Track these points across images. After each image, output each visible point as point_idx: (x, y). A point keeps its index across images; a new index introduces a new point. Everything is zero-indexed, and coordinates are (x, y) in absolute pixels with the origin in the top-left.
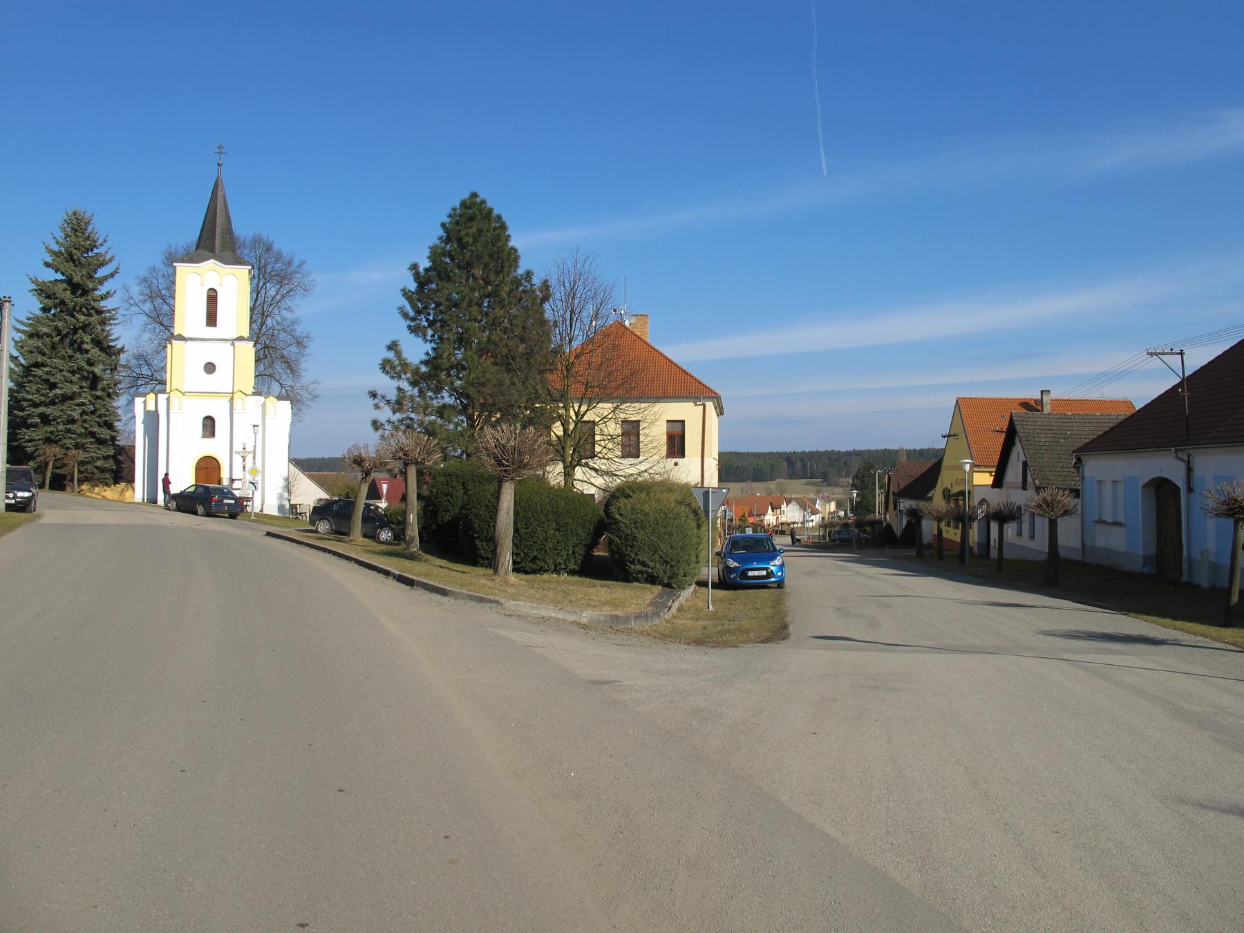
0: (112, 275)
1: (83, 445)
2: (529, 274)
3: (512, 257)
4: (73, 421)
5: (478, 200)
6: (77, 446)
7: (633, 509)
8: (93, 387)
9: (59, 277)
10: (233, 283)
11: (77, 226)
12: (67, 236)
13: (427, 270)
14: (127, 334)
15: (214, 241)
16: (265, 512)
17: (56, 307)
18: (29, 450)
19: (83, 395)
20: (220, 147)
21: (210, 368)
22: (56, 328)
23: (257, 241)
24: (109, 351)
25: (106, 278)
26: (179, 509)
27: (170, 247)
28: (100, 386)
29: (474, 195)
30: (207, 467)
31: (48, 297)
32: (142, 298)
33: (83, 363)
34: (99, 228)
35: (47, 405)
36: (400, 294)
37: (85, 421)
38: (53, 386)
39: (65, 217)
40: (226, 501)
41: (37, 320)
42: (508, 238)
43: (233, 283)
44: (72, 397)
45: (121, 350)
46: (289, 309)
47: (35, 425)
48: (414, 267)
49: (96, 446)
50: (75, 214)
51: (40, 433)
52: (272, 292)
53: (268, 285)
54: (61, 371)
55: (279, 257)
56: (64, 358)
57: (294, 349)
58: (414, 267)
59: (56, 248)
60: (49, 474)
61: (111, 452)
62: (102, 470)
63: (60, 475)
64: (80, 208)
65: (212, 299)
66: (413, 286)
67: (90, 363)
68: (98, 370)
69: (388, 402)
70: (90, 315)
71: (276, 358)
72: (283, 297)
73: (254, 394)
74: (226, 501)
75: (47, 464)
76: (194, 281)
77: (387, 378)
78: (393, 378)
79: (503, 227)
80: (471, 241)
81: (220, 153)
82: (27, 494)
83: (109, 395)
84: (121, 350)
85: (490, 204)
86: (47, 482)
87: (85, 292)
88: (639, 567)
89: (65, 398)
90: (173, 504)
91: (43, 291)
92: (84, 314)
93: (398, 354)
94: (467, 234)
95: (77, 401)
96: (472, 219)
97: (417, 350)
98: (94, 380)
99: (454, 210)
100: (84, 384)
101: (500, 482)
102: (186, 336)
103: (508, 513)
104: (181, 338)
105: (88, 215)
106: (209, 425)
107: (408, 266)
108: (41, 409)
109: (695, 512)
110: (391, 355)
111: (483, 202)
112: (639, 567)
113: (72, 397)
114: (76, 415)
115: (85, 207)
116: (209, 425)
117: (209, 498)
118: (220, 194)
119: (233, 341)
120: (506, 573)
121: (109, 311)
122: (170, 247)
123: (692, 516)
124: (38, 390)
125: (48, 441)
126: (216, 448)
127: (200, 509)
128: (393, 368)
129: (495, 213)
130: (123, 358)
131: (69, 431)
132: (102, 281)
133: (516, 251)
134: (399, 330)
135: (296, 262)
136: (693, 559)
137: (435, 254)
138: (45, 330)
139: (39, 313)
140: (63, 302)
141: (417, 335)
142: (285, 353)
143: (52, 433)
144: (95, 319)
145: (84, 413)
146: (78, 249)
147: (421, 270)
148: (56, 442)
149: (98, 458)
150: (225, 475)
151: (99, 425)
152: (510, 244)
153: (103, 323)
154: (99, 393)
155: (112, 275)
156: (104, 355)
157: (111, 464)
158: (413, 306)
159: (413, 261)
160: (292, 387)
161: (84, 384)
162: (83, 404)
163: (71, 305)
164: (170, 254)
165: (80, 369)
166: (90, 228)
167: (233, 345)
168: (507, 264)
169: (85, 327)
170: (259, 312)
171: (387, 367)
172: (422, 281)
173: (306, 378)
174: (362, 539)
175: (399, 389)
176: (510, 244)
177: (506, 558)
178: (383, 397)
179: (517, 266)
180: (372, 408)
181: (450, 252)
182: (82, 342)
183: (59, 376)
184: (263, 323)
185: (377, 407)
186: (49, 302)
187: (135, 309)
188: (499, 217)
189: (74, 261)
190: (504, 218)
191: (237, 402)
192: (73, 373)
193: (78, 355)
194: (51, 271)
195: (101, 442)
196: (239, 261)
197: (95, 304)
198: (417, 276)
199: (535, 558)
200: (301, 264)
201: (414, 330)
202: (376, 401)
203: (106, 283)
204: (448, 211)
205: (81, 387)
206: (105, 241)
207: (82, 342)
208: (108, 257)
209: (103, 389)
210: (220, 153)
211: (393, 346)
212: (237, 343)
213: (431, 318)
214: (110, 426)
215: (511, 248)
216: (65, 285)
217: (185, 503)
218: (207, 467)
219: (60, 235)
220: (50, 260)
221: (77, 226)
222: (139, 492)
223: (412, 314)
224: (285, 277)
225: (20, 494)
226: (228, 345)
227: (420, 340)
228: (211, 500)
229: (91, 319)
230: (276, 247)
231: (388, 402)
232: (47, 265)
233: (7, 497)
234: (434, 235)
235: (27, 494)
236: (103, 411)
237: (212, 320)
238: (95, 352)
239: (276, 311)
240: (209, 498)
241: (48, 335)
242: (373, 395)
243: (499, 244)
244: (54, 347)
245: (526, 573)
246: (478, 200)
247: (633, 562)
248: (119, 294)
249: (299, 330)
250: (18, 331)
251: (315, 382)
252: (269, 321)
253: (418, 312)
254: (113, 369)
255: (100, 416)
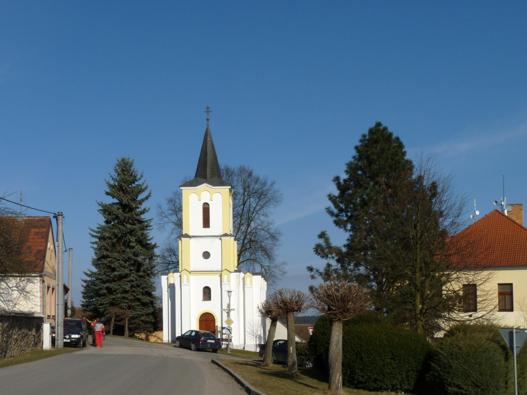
0: (147, 198)
1: (133, 307)
2: (420, 178)
3: (409, 166)
4: (126, 292)
5: (381, 128)
6: (130, 307)
7: (451, 344)
8: (138, 270)
9: (116, 201)
10: (219, 199)
11: (125, 169)
12: (119, 175)
13: (345, 180)
14: (157, 236)
15: (208, 171)
16: (246, 349)
17: (114, 221)
18: (101, 310)
19: (132, 275)
20: (208, 108)
21: (206, 255)
22: (114, 233)
23: (242, 170)
24: (149, 247)
25: (143, 200)
26: (181, 346)
27: (186, 178)
28: (142, 269)
29: (379, 124)
30: (207, 319)
31: (109, 214)
32: (170, 212)
33: (130, 255)
34: (138, 168)
35: (110, 282)
36: (327, 199)
37: (133, 292)
38: (114, 270)
39: (117, 163)
40: (209, 341)
41: (103, 229)
42: (404, 154)
43: (219, 199)
44: (126, 276)
45: (155, 246)
46: (266, 215)
47: (104, 295)
48: (337, 179)
49: (141, 307)
50: (123, 160)
51: (106, 300)
52: (254, 205)
53: (251, 199)
54: (118, 260)
55: (257, 180)
56: (119, 252)
57: (270, 241)
58: (337, 179)
59: (112, 182)
60: (112, 325)
61: (151, 310)
62: (146, 322)
63: (120, 326)
64: (126, 156)
65: (206, 209)
66: (336, 192)
67: (136, 255)
68: (140, 259)
69: (321, 274)
70: (135, 224)
71: (253, 249)
72: (262, 207)
73: (236, 271)
74: (209, 341)
75: (111, 318)
76: (194, 199)
77: (319, 257)
78: (322, 257)
79: (401, 146)
80: (375, 157)
81: (208, 112)
82: (77, 336)
83: (148, 275)
84: (155, 246)
85: (390, 130)
86: (111, 330)
87: (131, 210)
88: (455, 389)
89: (121, 277)
90: (178, 343)
91: (106, 210)
92: (130, 224)
93: (327, 240)
94: (373, 153)
95: (128, 279)
96: (376, 142)
97: (340, 238)
98: (138, 266)
99: (364, 136)
100: (132, 268)
101: (331, 322)
102: (190, 234)
103: (337, 345)
104: (187, 236)
105: (130, 160)
106: (207, 293)
107: (332, 178)
108: (107, 285)
109: (504, 348)
110: (321, 241)
111: (385, 129)
112: (455, 389)
113: (126, 276)
114: (128, 288)
115: (129, 155)
116: (207, 293)
117: (205, 339)
118: (209, 139)
119: (220, 237)
120: (337, 388)
121: (146, 221)
122: (186, 178)
123: (500, 350)
124: (105, 273)
125: (112, 304)
126: (213, 307)
127: (193, 346)
128: (323, 250)
129: (394, 136)
130: (157, 251)
131: (124, 298)
132: (140, 203)
133: (411, 162)
134: (328, 224)
135: (269, 183)
136: (503, 385)
137: (351, 169)
138: (107, 235)
139: (104, 224)
140: (117, 217)
141: (340, 227)
142: (263, 244)
143: (114, 299)
144: (137, 226)
145: (132, 286)
146: (125, 182)
147: (342, 181)
148: (117, 305)
149: (142, 315)
150: (218, 324)
151: (143, 294)
152: (406, 158)
153: (143, 229)
154: (141, 274)
155: (147, 198)
156: (144, 249)
157: (151, 319)
158: (337, 206)
159: (336, 174)
160: (269, 267)
161: (132, 268)
162: (132, 281)
163: (122, 218)
164: (261, 195)
165: (129, 258)
166: (132, 169)
167: (221, 239)
168: (403, 173)
169: (131, 232)
170: (242, 218)
171: (319, 250)
172: (343, 188)
173: (278, 260)
174: (272, 365)
175: (329, 265)
176: (406, 158)
177: (337, 377)
178: (317, 271)
179: (412, 174)
180: (310, 278)
181: (361, 167)
182: (130, 242)
183: (117, 264)
184: (249, 225)
185: (313, 277)
186: (110, 217)
187: (165, 220)
188: (397, 139)
189: (123, 190)
190: (402, 139)
191: (225, 277)
192: (126, 261)
193: (128, 250)
194: (110, 197)
195: (144, 305)
196: (222, 184)
197: (137, 217)
198: (339, 185)
199: (376, 380)
200: (273, 184)
201: (338, 223)
202: (312, 273)
203: (143, 204)
204: (360, 137)
205: (131, 270)
206: (142, 176)
207: (130, 242)
208: (143, 187)
209: (144, 271)
210: (208, 112)
211: (322, 235)
212: (223, 238)
213: (349, 214)
214: (149, 294)
215: (407, 161)
216: (118, 206)
217: (186, 342)
218: (207, 319)
219: (114, 174)
220: (108, 190)
221: (125, 169)
222: (166, 335)
223: (336, 211)
224: (262, 194)
225: (73, 336)
226: (217, 240)
227: (342, 230)
228: (199, 340)
229: (134, 227)
230: (255, 174)
231: (321, 274)
232: (108, 194)
233: (65, 338)
234: (349, 154)
235: (77, 336)
236: (144, 285)
237: (206, 223)
238: (138, 247)
239: (257, 217)
240: (205, 339)
241: (110, 238)
242: (311, 269)
243: (397, 158)
244: (113, 245)
245: (370, 390)
246: (381, 128)
247: (450, 385)
248: (151, 210)
249: (273, 229)
250: (93, 236)
251: (284, 263)
252: (253, 225)
253: (341, 210)
254: (151, 258)
255: (143, 288)
